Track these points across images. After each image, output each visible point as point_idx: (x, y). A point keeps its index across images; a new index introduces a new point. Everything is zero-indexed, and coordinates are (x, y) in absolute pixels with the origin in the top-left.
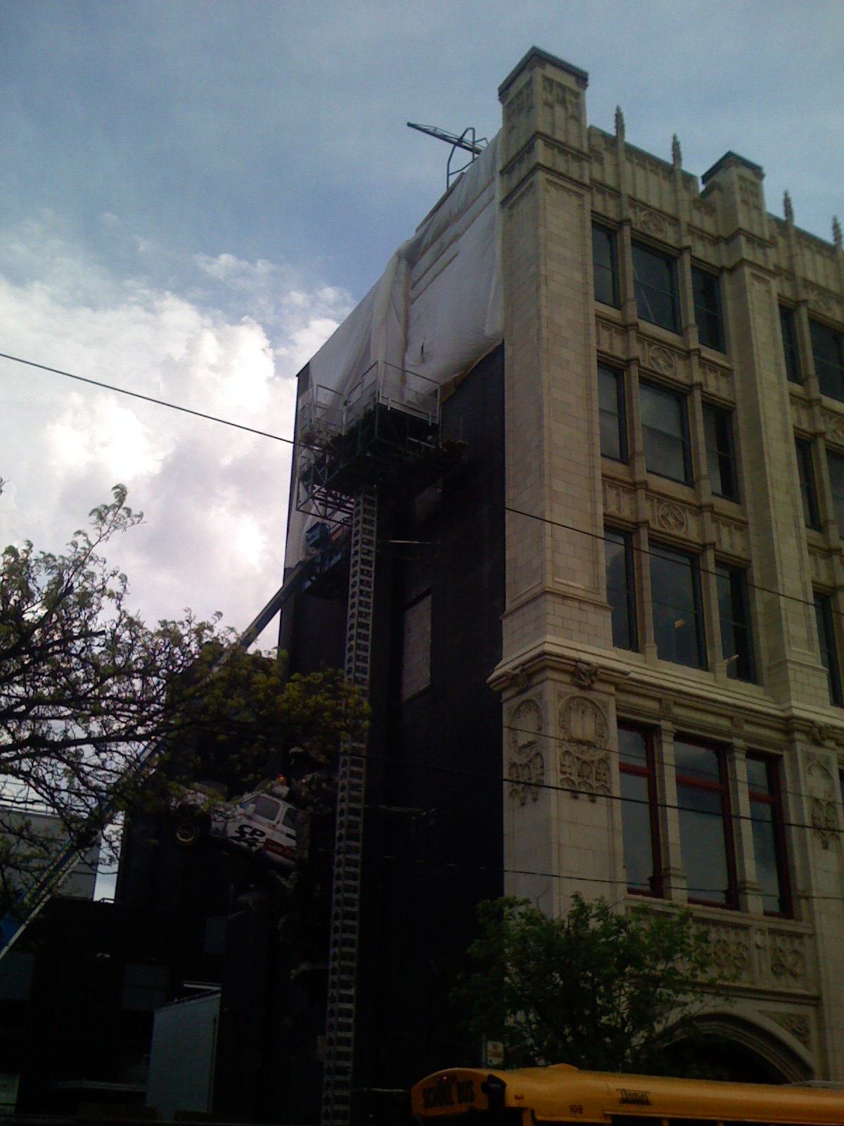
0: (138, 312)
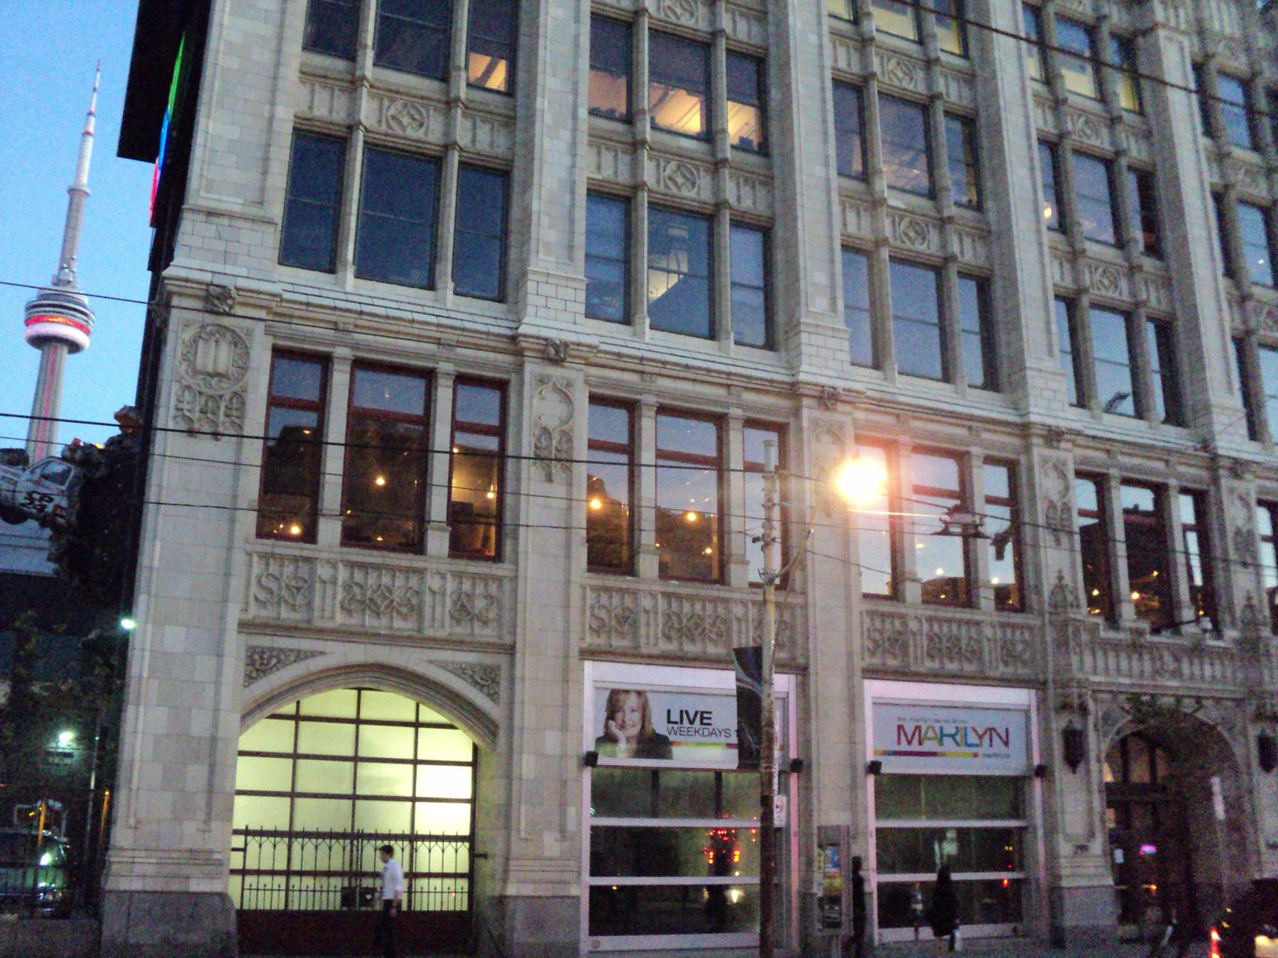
0: (640, 116)
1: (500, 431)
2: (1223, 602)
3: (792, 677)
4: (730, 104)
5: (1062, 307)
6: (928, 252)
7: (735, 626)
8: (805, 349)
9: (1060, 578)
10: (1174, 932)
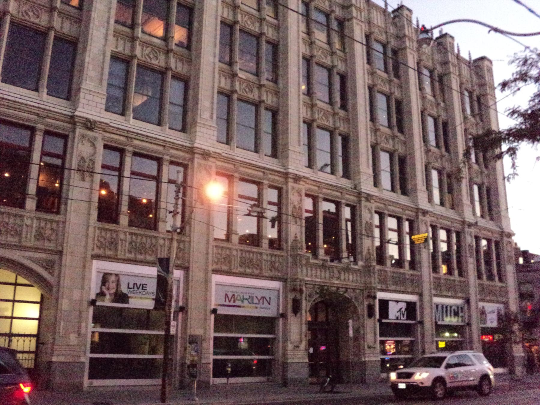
0: (235, 64)
1: (63, 157)
2: (359, 249)
3: (182, 272)
4: (176, 26)
5: (306, 126)
6: (253, 98)
7: (159, 248)
8: (82, 100)
9: (296, 237)
10: (330, 381)
